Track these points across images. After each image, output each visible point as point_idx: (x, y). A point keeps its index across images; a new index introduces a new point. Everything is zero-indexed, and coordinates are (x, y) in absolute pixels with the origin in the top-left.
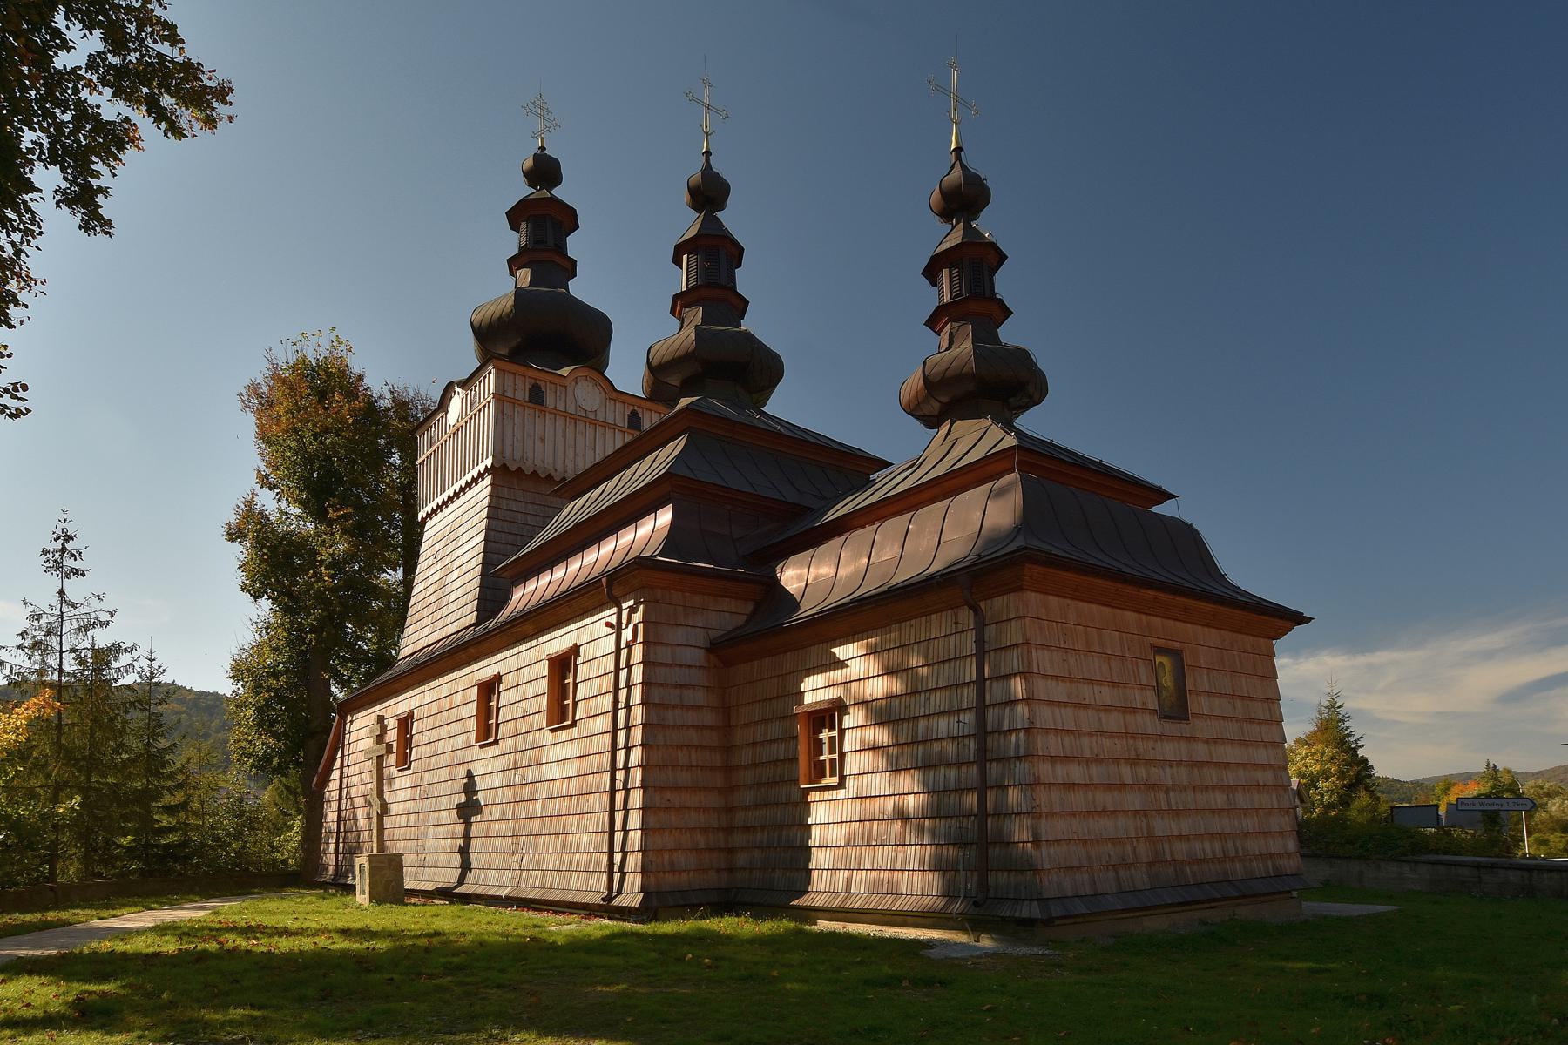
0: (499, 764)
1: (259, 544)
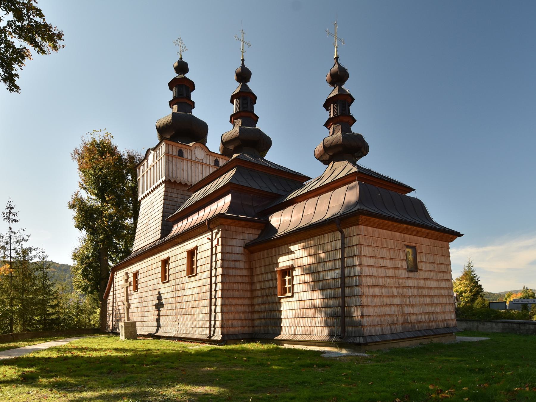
0: (170, 289)
1: (80, 210)
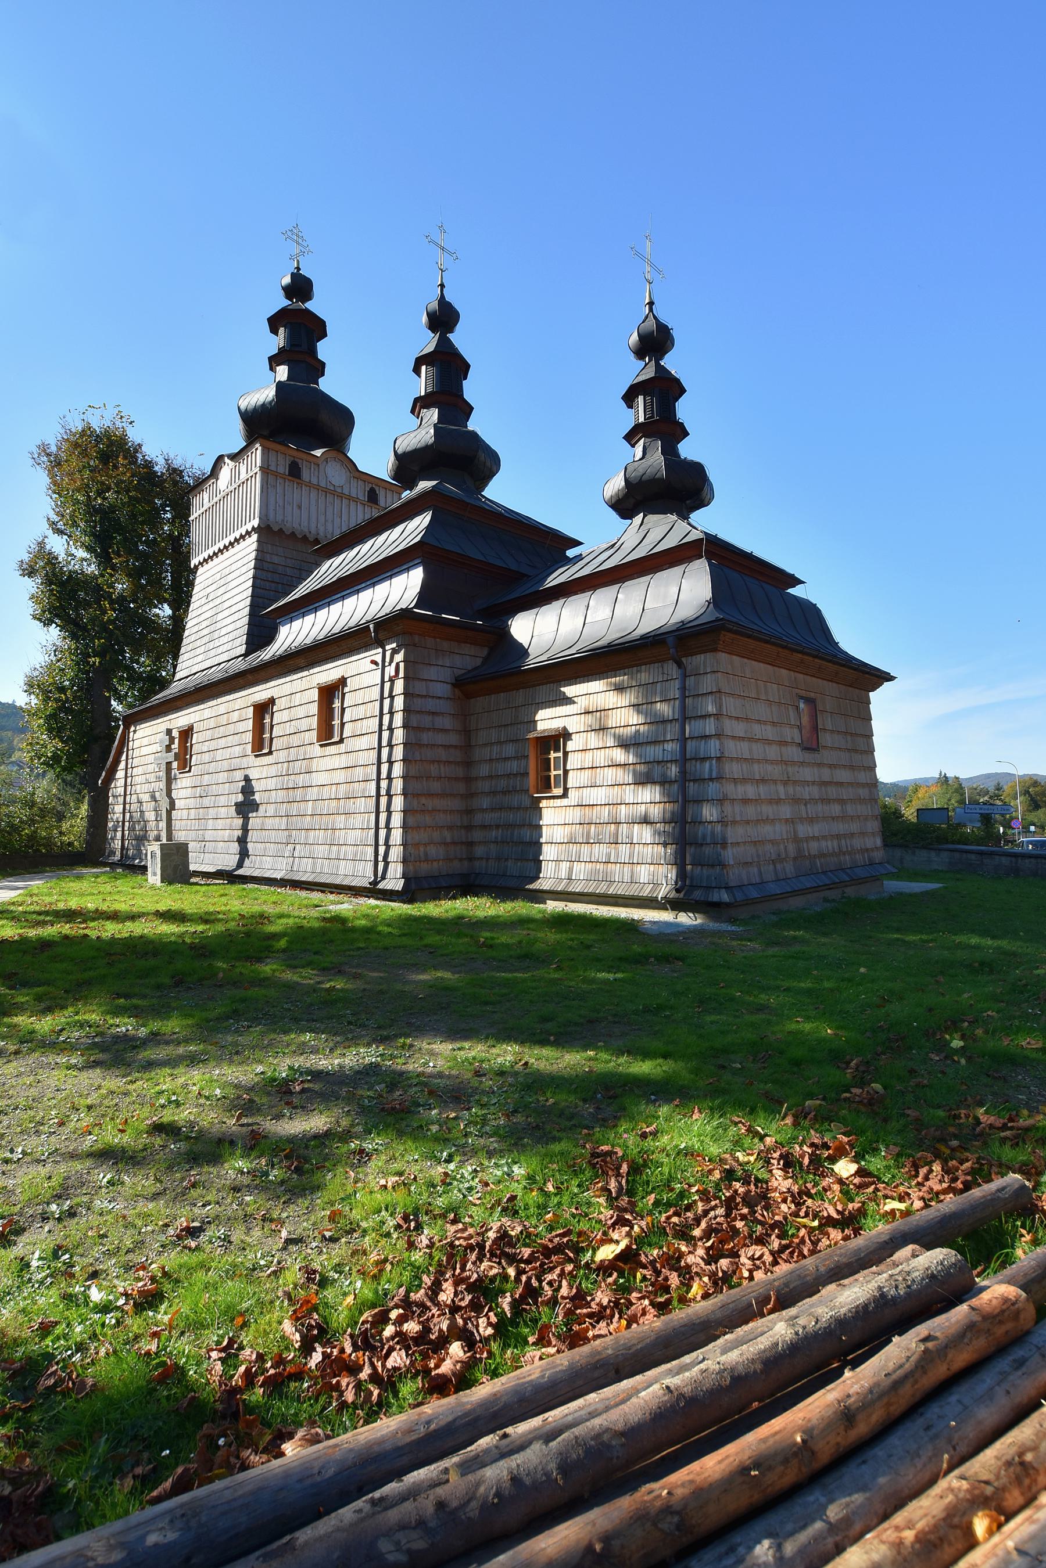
0: (273, 770)
1: (48, 581)
